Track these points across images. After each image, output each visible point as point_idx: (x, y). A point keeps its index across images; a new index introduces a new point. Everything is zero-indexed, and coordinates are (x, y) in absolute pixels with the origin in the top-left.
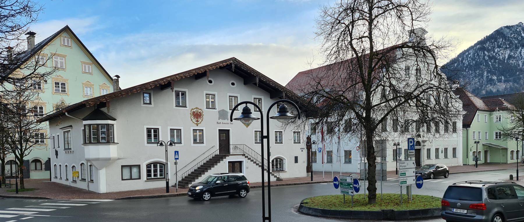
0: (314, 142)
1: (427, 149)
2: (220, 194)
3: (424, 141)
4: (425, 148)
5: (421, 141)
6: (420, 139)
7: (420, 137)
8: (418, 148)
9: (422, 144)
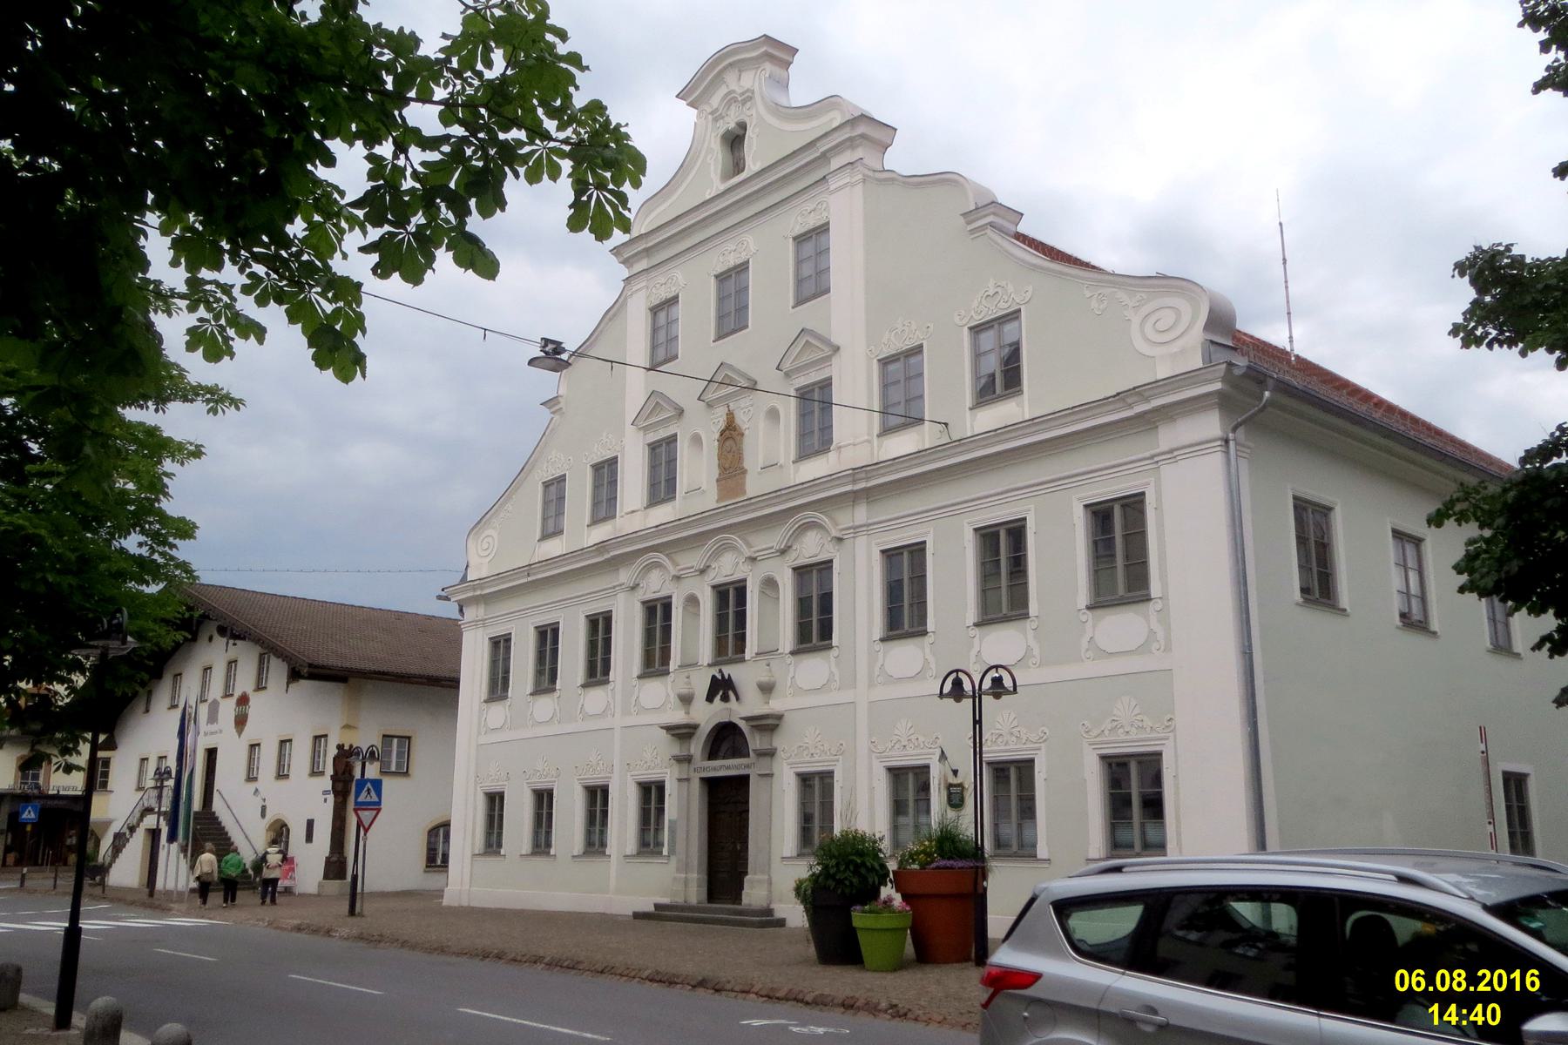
0: (997, 682)
1: (805, 780)
3: (768, 724)
4: (776, 770)
5: (742, 725)
6: (737, 711)
9: (755, 742)
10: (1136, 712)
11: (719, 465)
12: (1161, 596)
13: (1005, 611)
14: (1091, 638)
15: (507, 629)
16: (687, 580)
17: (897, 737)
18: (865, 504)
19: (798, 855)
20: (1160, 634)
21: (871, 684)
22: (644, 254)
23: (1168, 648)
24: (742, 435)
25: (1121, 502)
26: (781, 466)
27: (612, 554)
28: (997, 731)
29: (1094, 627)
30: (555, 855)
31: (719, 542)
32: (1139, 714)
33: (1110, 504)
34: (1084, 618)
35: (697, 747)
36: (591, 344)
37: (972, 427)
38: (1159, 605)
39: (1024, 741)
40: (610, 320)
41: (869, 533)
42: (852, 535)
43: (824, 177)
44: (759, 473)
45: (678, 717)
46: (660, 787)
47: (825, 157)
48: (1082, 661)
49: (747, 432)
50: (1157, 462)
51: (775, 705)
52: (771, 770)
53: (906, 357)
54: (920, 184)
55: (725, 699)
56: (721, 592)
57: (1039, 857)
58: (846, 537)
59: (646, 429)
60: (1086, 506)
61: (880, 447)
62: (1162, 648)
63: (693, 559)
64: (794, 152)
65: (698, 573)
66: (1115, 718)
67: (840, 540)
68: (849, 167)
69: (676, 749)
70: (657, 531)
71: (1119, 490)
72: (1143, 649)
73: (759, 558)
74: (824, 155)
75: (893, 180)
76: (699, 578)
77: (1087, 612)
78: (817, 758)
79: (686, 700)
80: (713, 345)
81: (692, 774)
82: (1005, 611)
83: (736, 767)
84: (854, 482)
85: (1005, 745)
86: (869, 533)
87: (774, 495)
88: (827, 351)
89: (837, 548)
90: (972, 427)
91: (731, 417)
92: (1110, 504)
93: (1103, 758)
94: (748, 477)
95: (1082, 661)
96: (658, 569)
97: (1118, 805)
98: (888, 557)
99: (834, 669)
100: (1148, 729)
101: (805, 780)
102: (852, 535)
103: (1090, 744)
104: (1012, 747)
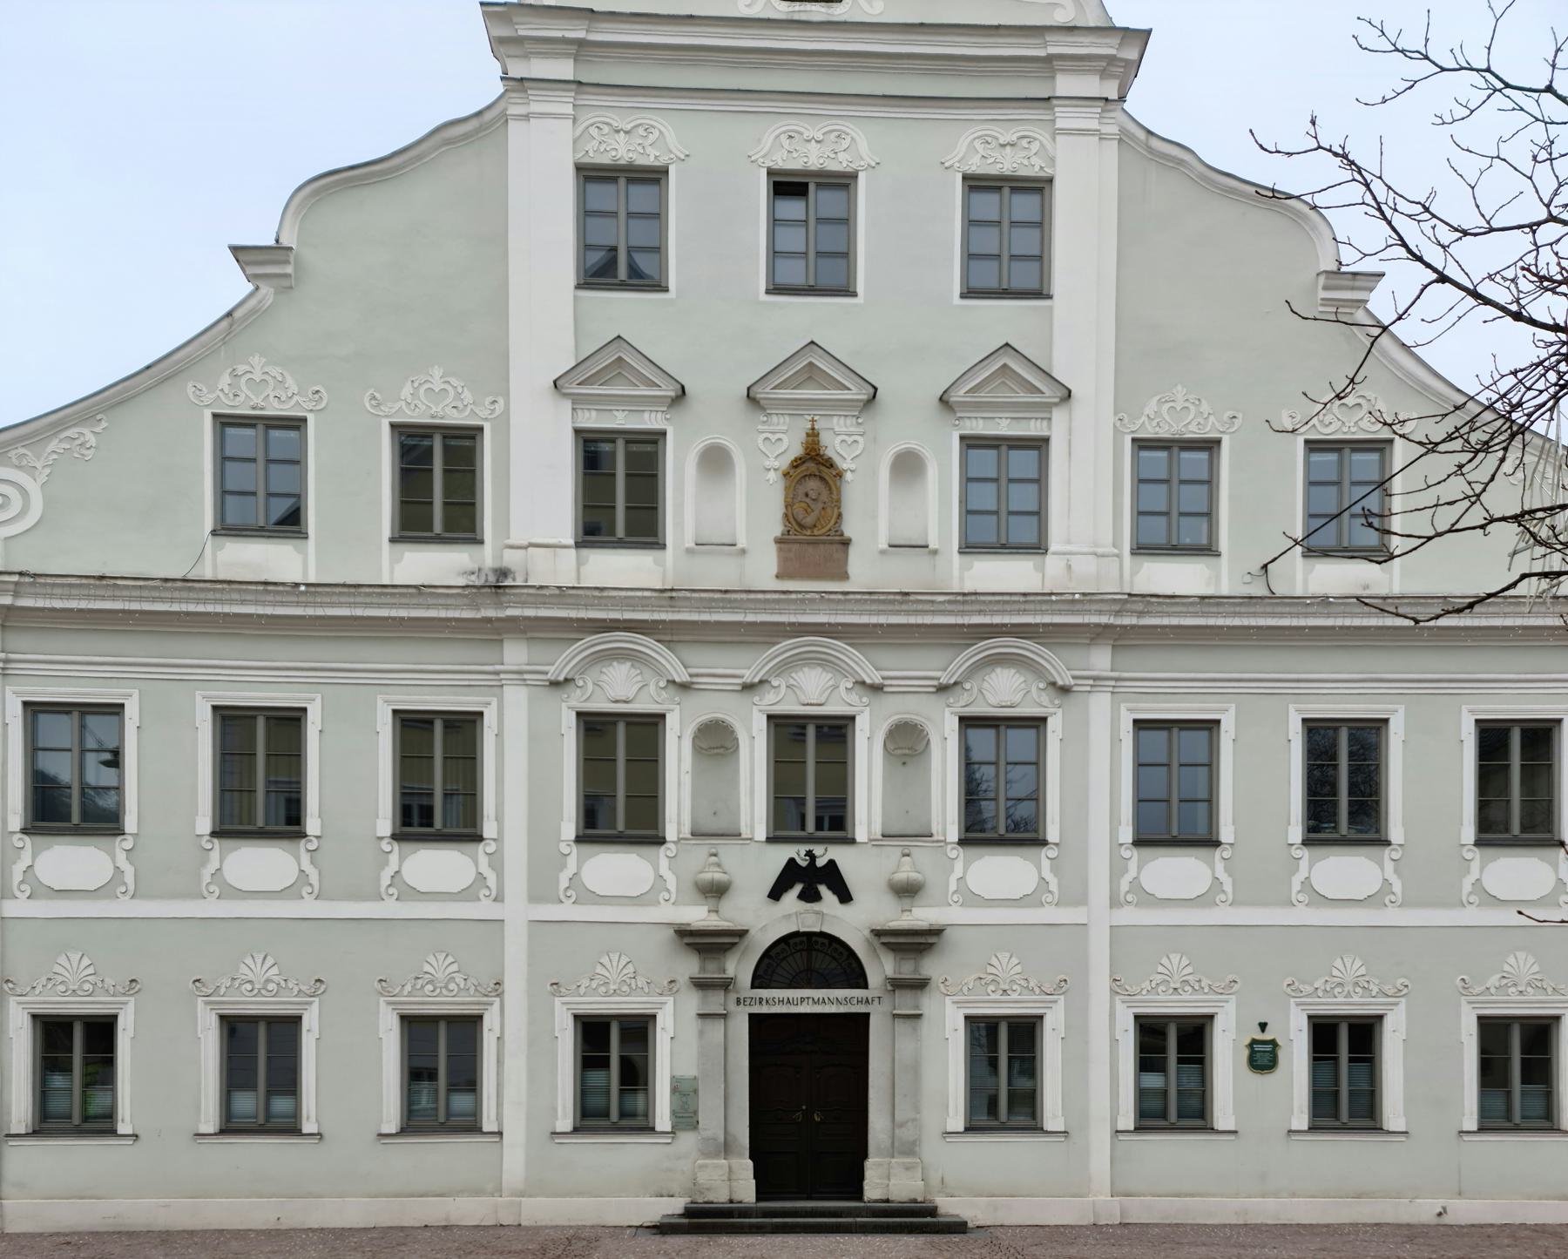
1: (982, 1030)
2: (785, 1224)
7: (845, 896)
8: (833, 1009)
9: (880, 967)
10: (82, 966)
11: (786, 515)
12: (495, 837)
13: (621, 826)
14: (397, 872)
15: (478, 703)
16: (891, 698)
17: (992, 976)
18: (1109, 649)
19: (1310, 1128)
20: (492, 880)
21: (1115, 902)
22: (573, 49)
23: (499, 898)
24: (840, 475)
25: (445, 717)
26: (935, 552)
27: (510, 612)
28: (1336, 979)
29: (1482, 869)
30: (500, 1134)
31: (809, 645)
32: (1537, 972)
33: (1509, 724)
34: (387, 848)
35: (740, 968)
36: (373, 174)
37: (1305, 582)
38: (492, 847)
39: (1374, 993)
40: (448, 142)
41: (1116, 690)
42: (1088, 688)
43: (1049, 98)
44: (883, 552)
45: (698, 915)
46: (639, 1029)
47: (1049, 64)
48: (1464, 906)
49: (848, 476)
50: (501, 680)
51: (921, 916)
52: (917, 1007)
53: (268, 427)
54: (1233, 191)
55: (810, 896)
56: (787, 730)
57: (119, 1133)
58: (1075, 689)
59: (578, 401)
60: (395, 712)
61: (1134, 574)
62: (672, 900)
63: (750, 664)
64: (998, 27)
65: (933, 690)
66: (1505, 975)
67: (1065, 690)
68: (1101, 103)
69: (690, 966)
70: (723, 600)
71: (1507, 711)
72: (467, 894)
73: (886, 689)
74: (1050, 59)
75: (1181, 162)
76: (933, 697)
77: (1475, 849)
78: (1014, 996)
79: (715, 891)
80: (764, 297)
81: (732, 1006)
82: (621, 826)
83: (847, 1001)
84: (1118, 613)
85: (1019, 995)
86: (1116, 690)
87: (78, 581)
88: (1050, 393)
89: (1057, 702)
90: (1305, 582)
91: (813, 435)
92: (1509, 724)
93: (35, 1017)
94: (854, 554)
95: (1464, 906)
96: (629, 664)
97: (417, 1074)
98: (224, 718)
99: (664, 869)
100: (1550, 990)
101: (982, 1030)
102: (1111, 689)
103: (1469, 1003)
104: (1356, 999)
